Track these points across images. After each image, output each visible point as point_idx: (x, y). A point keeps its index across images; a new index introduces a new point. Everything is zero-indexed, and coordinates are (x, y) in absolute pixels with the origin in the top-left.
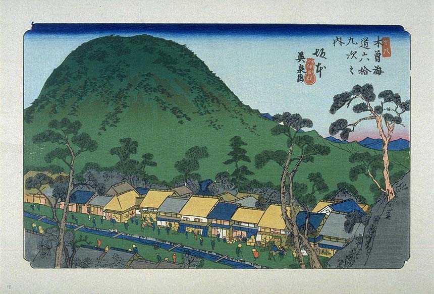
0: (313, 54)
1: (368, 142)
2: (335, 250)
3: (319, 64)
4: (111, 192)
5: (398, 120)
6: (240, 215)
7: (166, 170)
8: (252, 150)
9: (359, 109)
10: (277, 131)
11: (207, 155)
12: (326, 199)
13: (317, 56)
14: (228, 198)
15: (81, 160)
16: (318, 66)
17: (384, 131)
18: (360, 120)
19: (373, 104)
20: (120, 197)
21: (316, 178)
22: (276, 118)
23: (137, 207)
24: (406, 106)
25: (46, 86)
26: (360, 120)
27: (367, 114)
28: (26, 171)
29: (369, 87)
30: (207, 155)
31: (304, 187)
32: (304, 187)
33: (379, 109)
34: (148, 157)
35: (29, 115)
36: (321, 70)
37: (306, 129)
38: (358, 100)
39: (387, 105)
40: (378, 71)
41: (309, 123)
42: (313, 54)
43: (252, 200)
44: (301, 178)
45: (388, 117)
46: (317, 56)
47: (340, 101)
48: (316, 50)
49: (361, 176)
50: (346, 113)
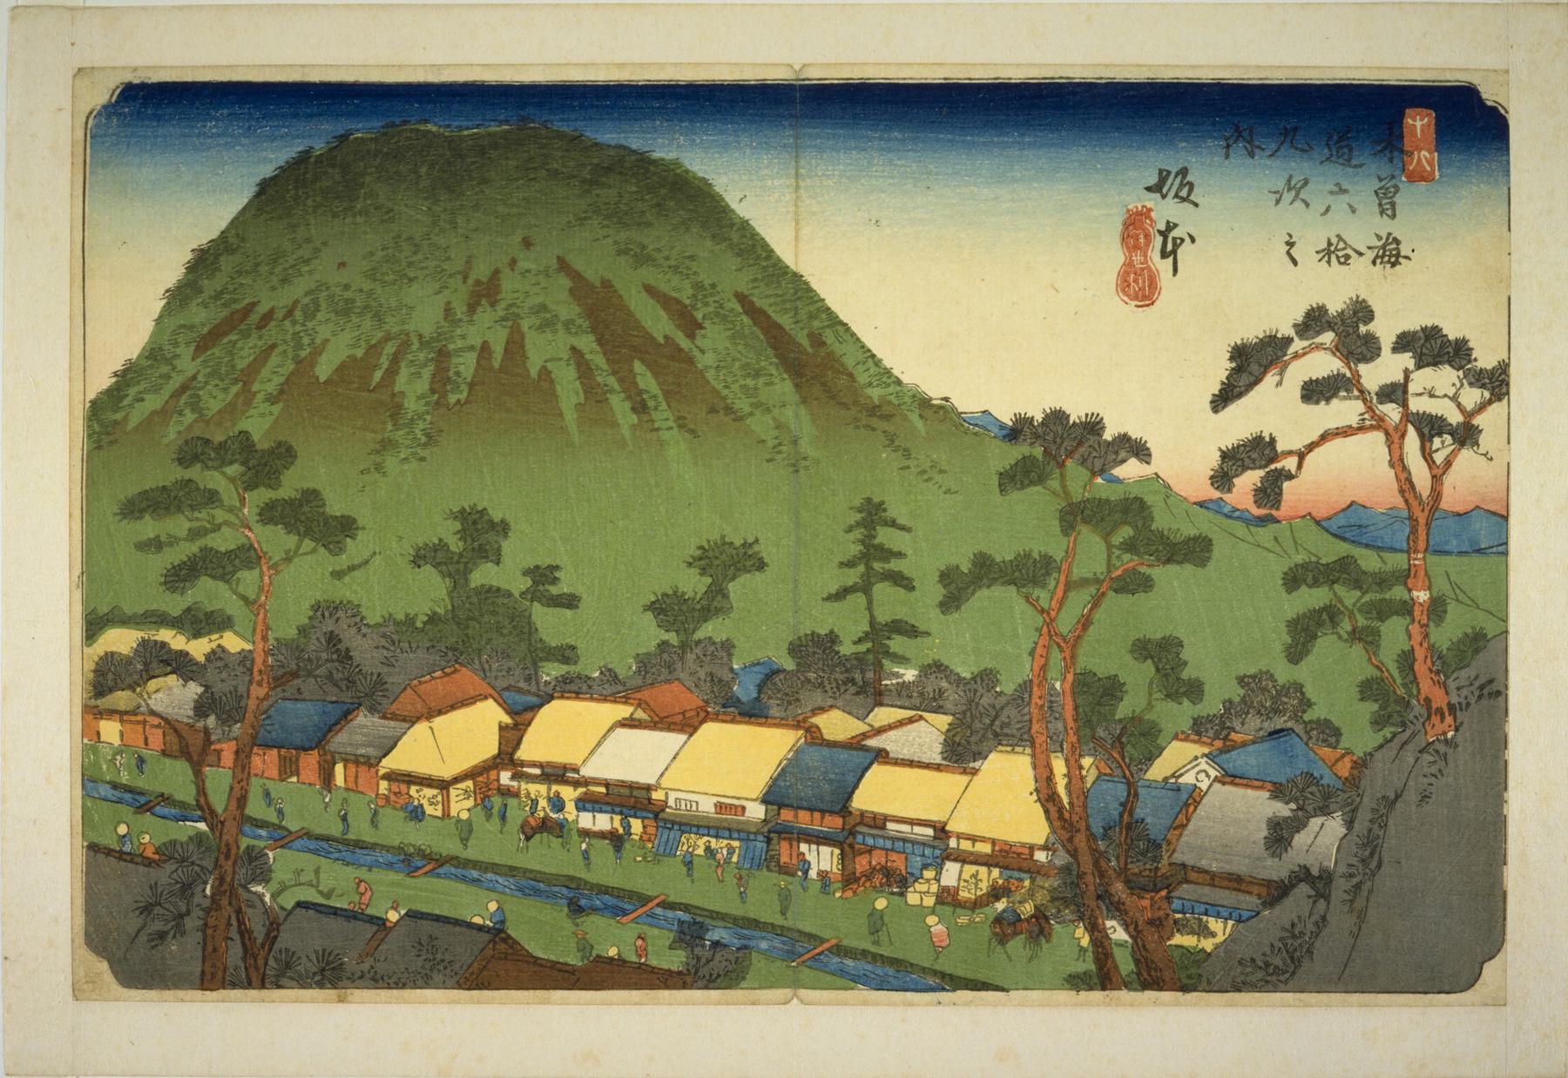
0: (1148, 189)
1: (1350, 523)
2: (1230, 923)
3: (1170, 227)
4: (407, 702)
5: (1466, 435)
6: (878, 792)
7: (619, 633)
8: (926, 551)
9: (1315, 392)
10: (1017, 477)
11: (761, 565)
12: (1199, 729)
13: (1164, 197)
14: (837, 724)
15: (299, 584)
16: (1164, 234)
17: (1477, 560)
18: (1325, 437)
19: (1375, 375)
20: (438, 721)
21: (1162, 654)
22: (1017, 431)
23: (506, 756)
24: (1496, 383)
25: (339, 979)
26: (1325, 437)
27: (1345, 410)
28: (94, 625)
29: (1361, 311)
30: (761, 565)
31: (1112, 689)
32: (1112, 689)
33: (1395, 392)
34: (542, 576)
35: (106, 421)
36: (1176, 246)
37: (1130, 470)
38: (1323, 364)
39: (1424, 378)
40: (1390, 254)
41: (1140, 451)
42: (1148, 189)
43: (927, 735)
44: (1105, 654)
45: (1430, 427)
46: (1164, 197)
47: (1252, 363)
48: (1161, 171)
49: (1327, 646)
50: (1275, 409)
